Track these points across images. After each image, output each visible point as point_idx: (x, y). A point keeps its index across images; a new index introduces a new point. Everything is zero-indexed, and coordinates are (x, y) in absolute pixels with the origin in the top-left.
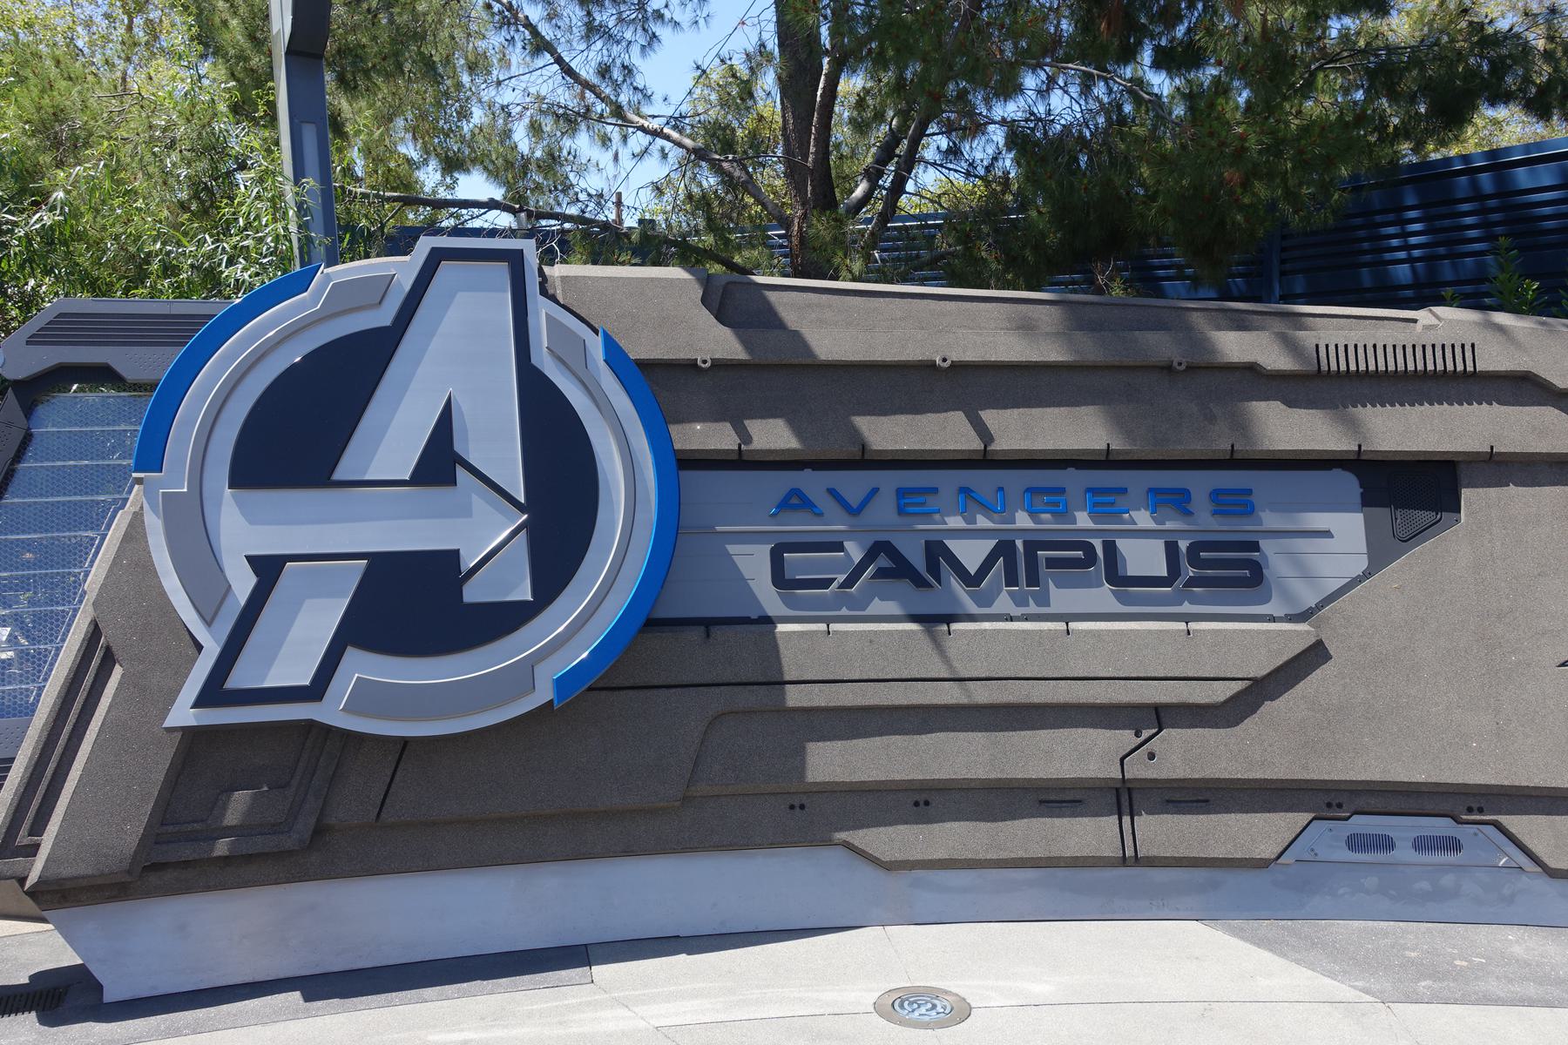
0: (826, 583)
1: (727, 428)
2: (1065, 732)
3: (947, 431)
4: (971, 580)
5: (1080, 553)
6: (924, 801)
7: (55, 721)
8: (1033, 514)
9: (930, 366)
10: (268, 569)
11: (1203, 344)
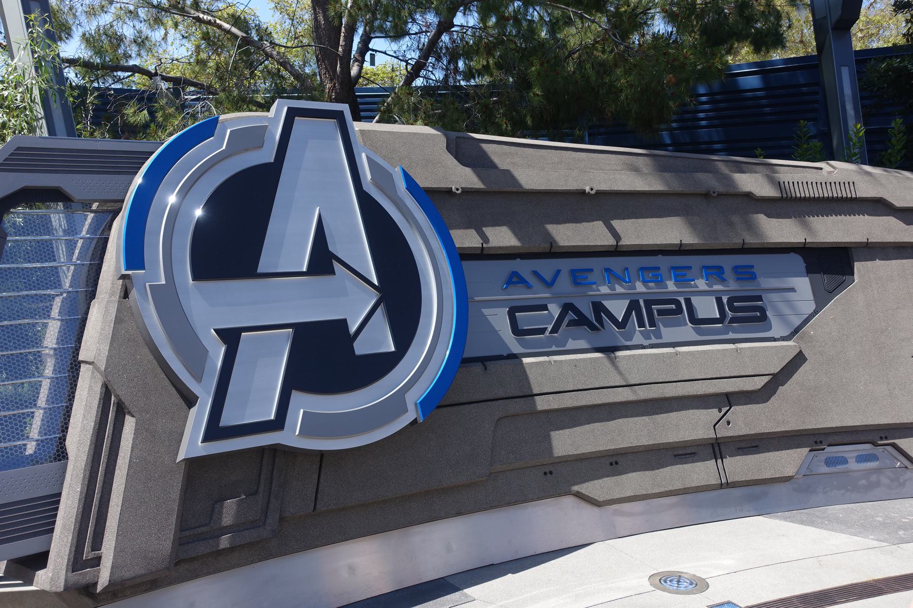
0: (542, 331)
1: (472, 232)
2: (683, 413)
3: (593, 234)
4: (621, 325)
5: (673, 306)
6: (615, 462)
7: (93, 461)
8: (645, 282)
9: (582, 193)
10: (230, 337)
11: (730, 182)
